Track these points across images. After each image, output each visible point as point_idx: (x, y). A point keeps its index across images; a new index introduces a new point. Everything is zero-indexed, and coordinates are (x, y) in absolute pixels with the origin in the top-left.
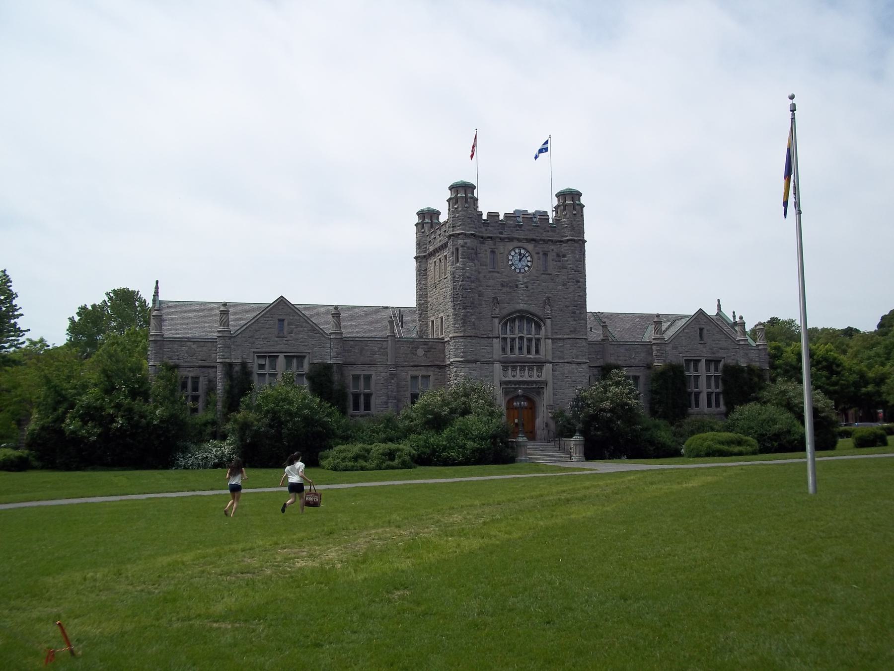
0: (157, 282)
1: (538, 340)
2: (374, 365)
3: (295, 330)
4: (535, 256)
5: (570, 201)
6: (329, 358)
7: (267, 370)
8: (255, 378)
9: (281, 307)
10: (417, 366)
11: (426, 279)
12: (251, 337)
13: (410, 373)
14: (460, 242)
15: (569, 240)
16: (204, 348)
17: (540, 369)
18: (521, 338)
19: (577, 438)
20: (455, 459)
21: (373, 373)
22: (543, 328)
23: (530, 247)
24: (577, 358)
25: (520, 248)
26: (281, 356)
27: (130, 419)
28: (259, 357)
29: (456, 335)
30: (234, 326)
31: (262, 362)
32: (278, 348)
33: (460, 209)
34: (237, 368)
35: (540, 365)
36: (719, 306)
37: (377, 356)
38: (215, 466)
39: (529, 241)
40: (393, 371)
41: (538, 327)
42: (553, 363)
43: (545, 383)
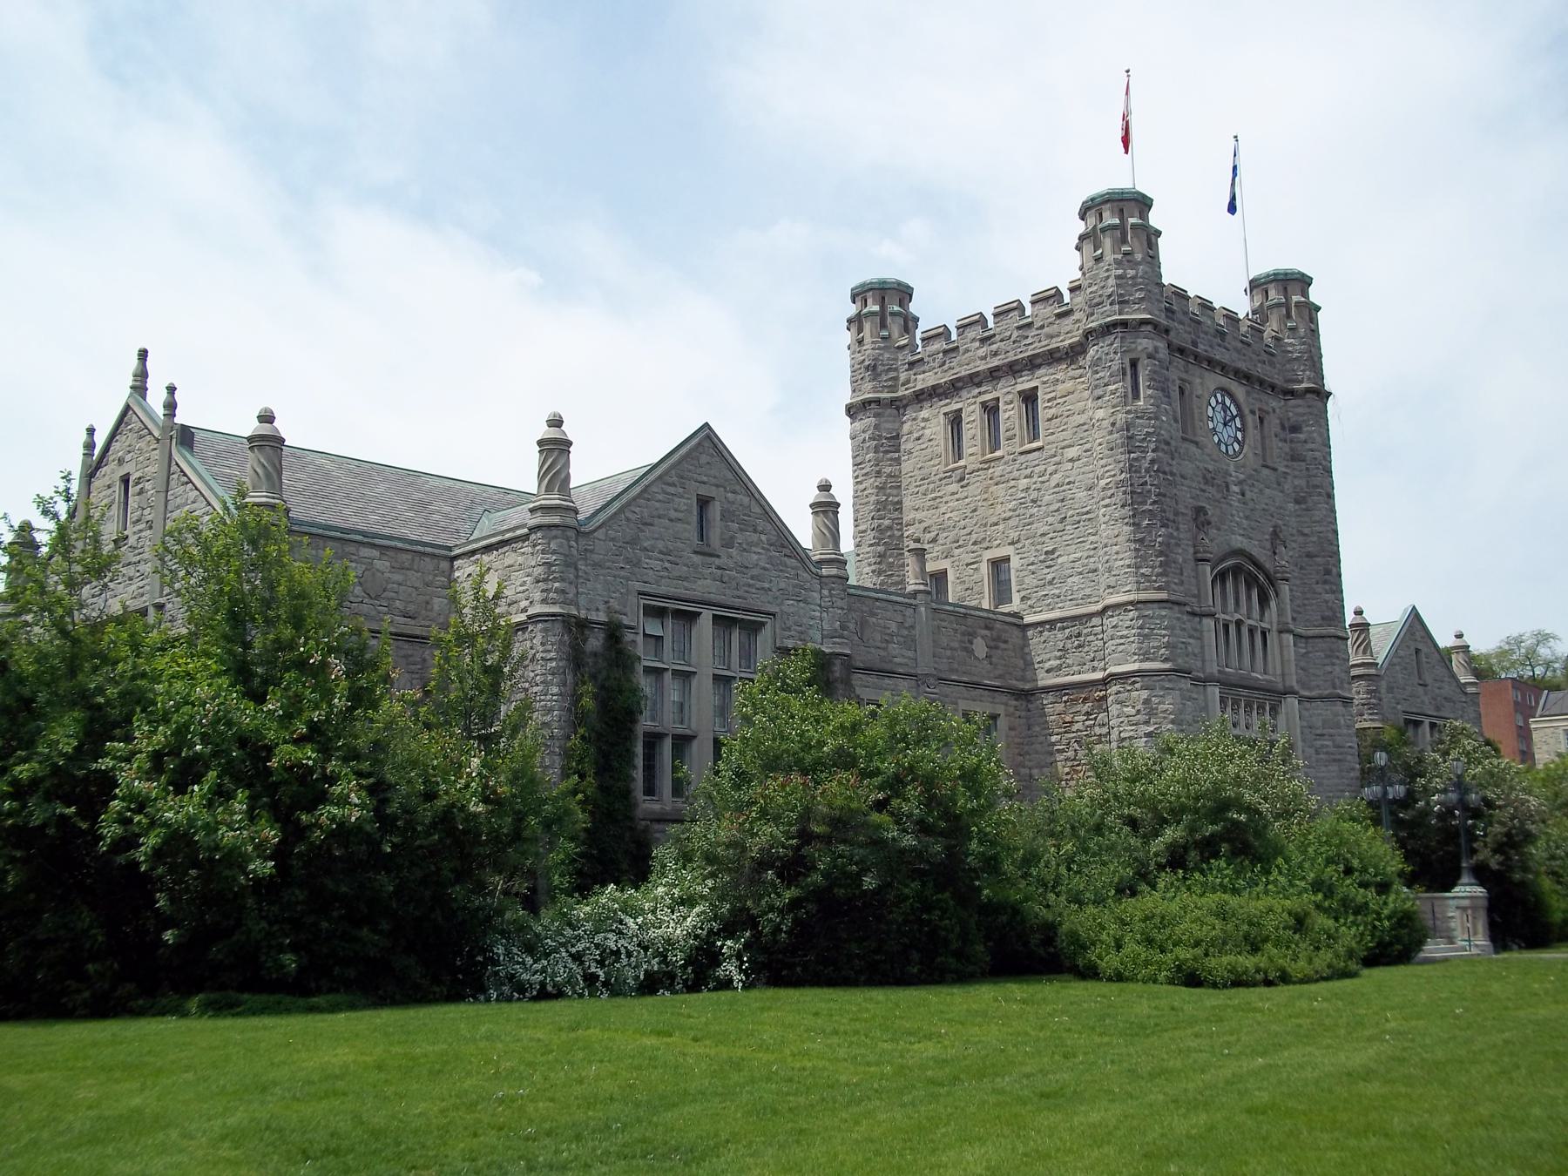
0: (143, 355)
2: (890, 673)
3: (740, 538)
4: (1249, 418)
5: (1287, 293)
6: (818, 637)
10: (975, 685)
11: (898, 461)
12: (633, 542)
13: (963, 705)
14: (1144, 343)
15: (1308, 390)
16: (413, 577)
18: (1239, 623)
19: (1468, 890)
22: (1273, 604)
23: (1239, 391)
25: (1226, 391)
27: (378, 790)
29: (1143, 596)
32: (705, 587)
33: (1138, 257)
34: (595, 642)
37: (894, 648)
38: (650, 985)
39: (1245, 377)
41: (1264, 601)
42: (1303, 700)
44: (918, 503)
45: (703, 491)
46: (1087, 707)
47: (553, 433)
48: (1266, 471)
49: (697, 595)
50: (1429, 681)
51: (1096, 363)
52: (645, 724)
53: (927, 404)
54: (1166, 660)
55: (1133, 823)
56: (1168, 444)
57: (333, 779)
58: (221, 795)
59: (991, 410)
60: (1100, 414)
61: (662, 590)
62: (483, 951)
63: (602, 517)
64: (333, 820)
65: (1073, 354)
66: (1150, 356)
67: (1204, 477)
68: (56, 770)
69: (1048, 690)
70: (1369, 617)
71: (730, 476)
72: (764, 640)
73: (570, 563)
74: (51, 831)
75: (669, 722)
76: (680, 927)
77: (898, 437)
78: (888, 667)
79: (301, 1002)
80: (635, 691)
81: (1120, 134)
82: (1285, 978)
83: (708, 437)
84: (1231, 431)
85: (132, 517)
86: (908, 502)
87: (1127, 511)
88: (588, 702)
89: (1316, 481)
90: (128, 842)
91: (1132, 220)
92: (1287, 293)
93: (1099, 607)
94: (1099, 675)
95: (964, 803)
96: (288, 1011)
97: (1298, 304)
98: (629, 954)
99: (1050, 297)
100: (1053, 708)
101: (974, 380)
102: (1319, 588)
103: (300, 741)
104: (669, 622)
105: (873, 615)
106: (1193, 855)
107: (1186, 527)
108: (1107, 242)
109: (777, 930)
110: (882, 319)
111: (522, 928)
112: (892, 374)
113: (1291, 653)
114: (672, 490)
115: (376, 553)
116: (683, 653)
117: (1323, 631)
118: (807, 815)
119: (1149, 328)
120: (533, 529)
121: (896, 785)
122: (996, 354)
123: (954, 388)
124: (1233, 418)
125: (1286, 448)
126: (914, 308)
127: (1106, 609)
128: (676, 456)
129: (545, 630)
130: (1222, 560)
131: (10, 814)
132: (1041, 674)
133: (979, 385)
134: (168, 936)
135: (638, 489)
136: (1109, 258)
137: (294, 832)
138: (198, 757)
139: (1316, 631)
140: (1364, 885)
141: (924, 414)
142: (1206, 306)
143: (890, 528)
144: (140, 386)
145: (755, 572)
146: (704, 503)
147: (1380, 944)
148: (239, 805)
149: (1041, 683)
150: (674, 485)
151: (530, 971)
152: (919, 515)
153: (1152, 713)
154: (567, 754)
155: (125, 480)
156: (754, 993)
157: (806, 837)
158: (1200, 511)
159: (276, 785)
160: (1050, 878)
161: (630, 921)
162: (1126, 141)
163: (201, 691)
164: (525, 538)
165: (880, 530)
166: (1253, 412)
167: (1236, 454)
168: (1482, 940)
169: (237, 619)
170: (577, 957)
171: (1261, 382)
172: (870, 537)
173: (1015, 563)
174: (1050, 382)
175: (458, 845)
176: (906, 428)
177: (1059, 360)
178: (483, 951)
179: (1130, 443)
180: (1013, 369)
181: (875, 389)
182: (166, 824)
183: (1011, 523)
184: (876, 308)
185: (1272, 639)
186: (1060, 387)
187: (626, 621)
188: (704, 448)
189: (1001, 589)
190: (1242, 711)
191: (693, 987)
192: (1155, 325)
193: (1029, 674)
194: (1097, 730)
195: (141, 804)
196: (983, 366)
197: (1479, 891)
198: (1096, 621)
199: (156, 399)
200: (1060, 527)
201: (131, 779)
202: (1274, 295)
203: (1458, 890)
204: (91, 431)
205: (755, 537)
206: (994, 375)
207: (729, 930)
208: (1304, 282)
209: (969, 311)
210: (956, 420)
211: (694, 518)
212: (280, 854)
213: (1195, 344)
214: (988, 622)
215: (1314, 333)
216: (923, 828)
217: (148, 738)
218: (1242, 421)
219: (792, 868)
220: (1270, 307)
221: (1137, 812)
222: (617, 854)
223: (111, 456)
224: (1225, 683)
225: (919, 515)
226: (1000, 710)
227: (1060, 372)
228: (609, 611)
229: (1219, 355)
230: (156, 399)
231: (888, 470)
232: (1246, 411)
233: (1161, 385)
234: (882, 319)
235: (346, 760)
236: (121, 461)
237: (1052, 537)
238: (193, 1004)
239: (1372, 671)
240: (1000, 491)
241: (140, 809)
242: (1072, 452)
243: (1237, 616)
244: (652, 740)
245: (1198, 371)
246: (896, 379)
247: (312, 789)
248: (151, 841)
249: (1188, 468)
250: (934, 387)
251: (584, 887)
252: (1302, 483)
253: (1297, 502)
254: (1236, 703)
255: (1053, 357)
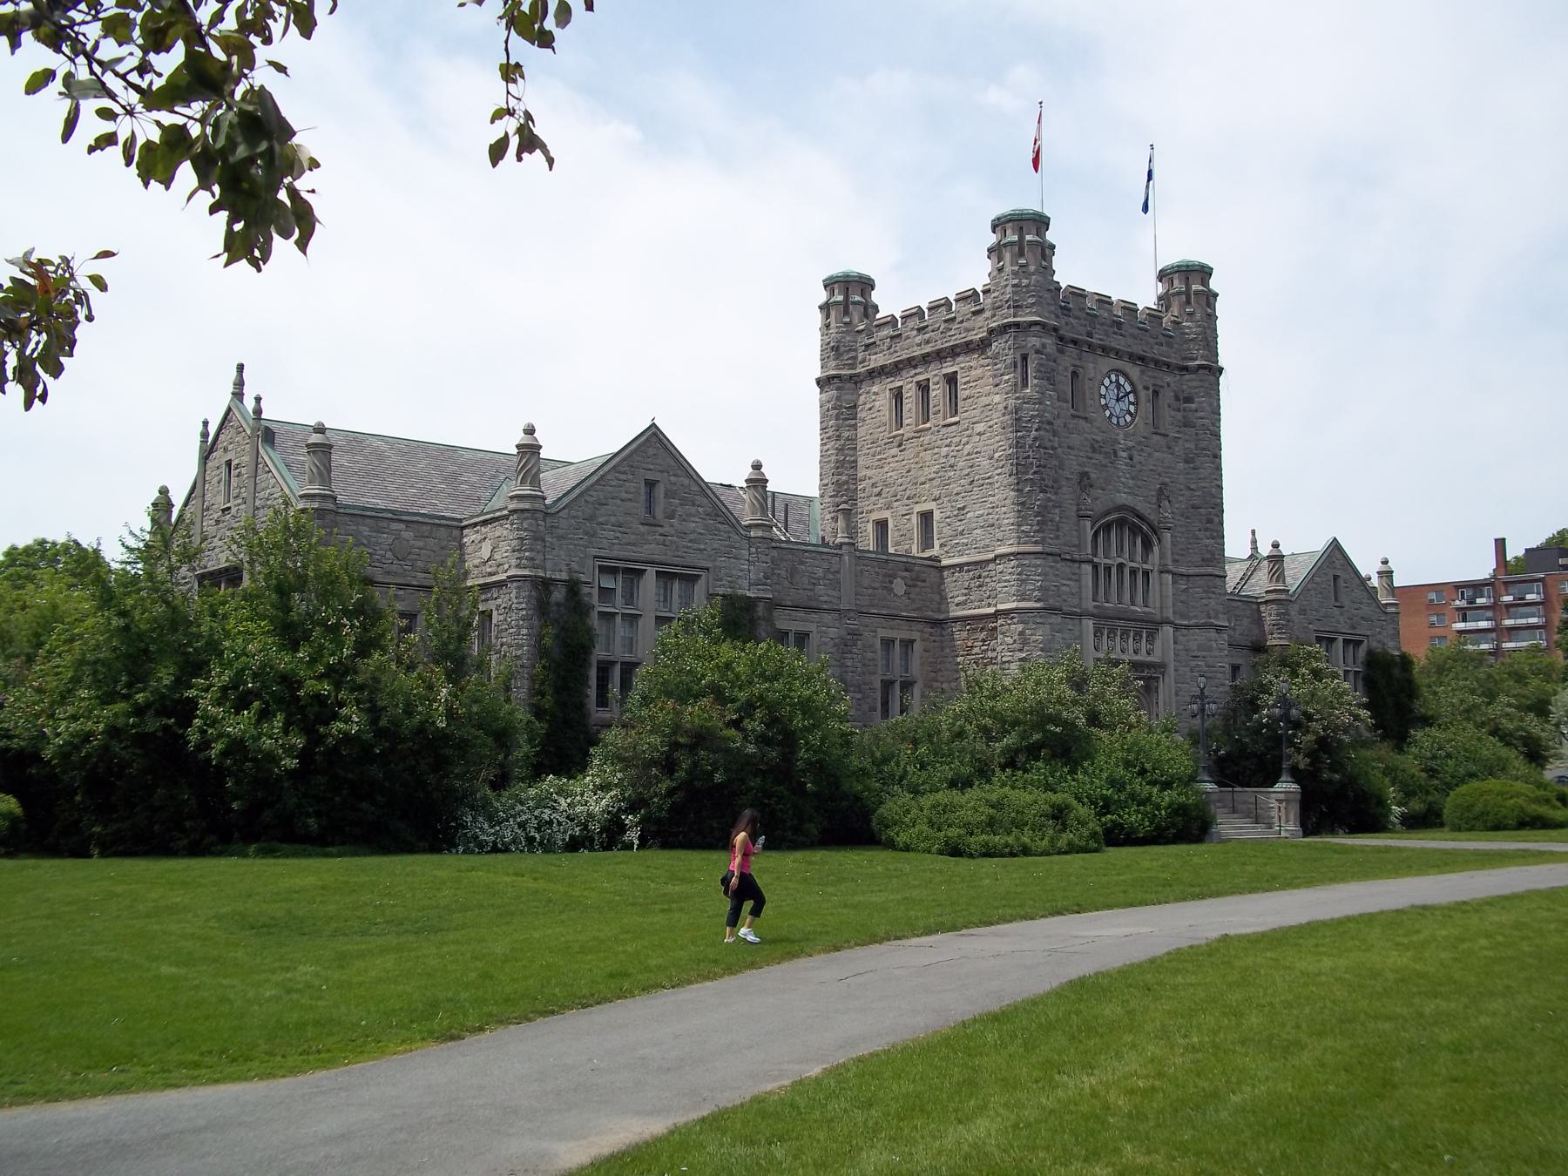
0: (241, 368)
1: (1146, 574)
3: (680, 511)
4: (1142, 394)
5: (1190, 285)
6: (745, 584)
7: (618, 606)
8: (594, 620)
9: (651, 451)
11: (855, 427)
12: (590, 518)
13: (882, 633)
14: (1034, 341)
15: (1201, 367)
16: (431, 541)
17: (1151, 638)
18: (1121, 566)
19: (1286, 786)
20: (1133, 830)
21: (812, 627)
22: (1156, 549)
23: (1134, 371)
24: (1216, 618)
25: (1119, 372)
26: (651, 572)
27: (374, 712)
28: (603, 569)
29: (1023, 548)
30: (553, 487)
31: (608, 582)
32: (650, 550)
33: (1032, 268)
34: (558, 595)
35: (1152, 626)
36: (1254, 542)
37: (820, 589)
38: (574, 845)
40: (854, 624)
41: (1147, 545)
42: (1177, 627)
43: (1161, 667)
44: (868, 463)
45: (650, 476)
46: (983, 635)
47: (528, 440)
48: (1156, 437)
49: (643, 556)
50: (1347, 603)
51: (996, 356)
52: (599, 653)
53: (877, 380)
54: (1038, 600)
55: (986, 731)
56: (1050, 423)
57: (341, 705)
58: (264, 715)
59: (924, 388)
60: (997, 398)
61: (614, 554)
62: (455, 819)
63: (566, 501)
64: (339, 732)
65: (982, 346)
66: (1037, 352)
67: (1092, 447)
68: (163, 696)
69: (956, 620)
70: (1285, 550)
71: (672, 463)
72: (700, 588)
73: (537, 538)
74: (160, 734)
75: (619, 653)
76: (599, 805)
77: (855, 406)
78: (814, 604)
79: (319, 850)
80: (589, 630)
81: (1031, 156)
82: (1026, 851)
83: (655, 434)
84: (1123, 405)
85: (234, 493)
86: (861, 462)
87: (1013, 479)
88: (548, 641)
89: (1203, 444)
90: (205, 744)
91: (1028, 237)
92: (1190, 285)
93: (991, 556)
94: (992, 610)
95: (798, 722)
96: (310, 855)
97: (1197, 293)
98: (559, 824)
99: (969, 297)
100: (960, 635)
101: (911, 363)
102: (1201, 535)
103: (320, 678)
104: (620, 578)
105: (802, 563)
106: (1022, 758)
107: (1067, 493)
108: (1007, 256)
109: (660, 809)
110: (846, 307)
111: (486, 803)
112: (852, 354)
113: (1170, 590)
114: (623, 477)
115: (402, 526)
116: (630, 598)
117: (1202, 570)
118: (677, 728)
119: (1038, 328)
120: (513, 512)
121: (749, 708)
122: (928, 342)
123: (896, 369)
124: (1127, 394)
125: (1179, 415)
126: (875, 297)
127: (996, 557)
128: (634, 446)
129: (518, 588)
130: (1107, 513)
131: (133, 726)
132: (952, 607)
133: (915, 367)
134: (234, 806)
135: (595, 478)
136: (1008, 269)
137: (314, 739)
138: (250, 692)
139: (1196, 571)
140: (1153, 783)
141: (875, 389)
142: (1104, 301)
143: (846, 482)
144: (238, 394)
145: (692, 537)
146: (651, 485)
147: (1158, 828)
148: (278, 722)
149: (952, 614)
150: (624, 473)
151: (487, 834)
152: (869, 473)
153: (1025, 642)
154: (532, 679)
155: (229, 463)
156: (648, 853)
157: (675, 746)
158: (1084, 475)
159: (304, 707)
160: (899, 772)
161: (562, 800)
162: (1036, 163)
163: (252, 645)
164: (506, 517)
165: (838, 484)
166: (1146, 388)
167: (1127, 425)
168: (1291, 827)
169: (283, 591)
170: (522, 825)
171: (1157, 362)
172: (830, 490)
173: (937, 516)
174: (971, 369)
175: (435, 748)
176: (862, 399)
177: (973, 351)
178: (455, 819)
179: (1018, 423)
180: (940, 356)
181: (837, 367)
182: (229, 735)
183: (935, 483)
184: (840, 298)
185: (1154, 577)
186: (974, 373)
187: (583, 578)
188: (653, 442)
189: (927, 542)
190: (1118, 639)
191: (607, 847)
192: (1043, 325)
193: (943, 607)
194: (990, 654)
195: (214, 722)
196: (918, 352)
197: (1294, 787)
198: (991, 566)
199: (249, 404)
200: (969, 488)
201: (206, 705)
202: (1178, 285)
203: (1279, 787)
204: (206, 423)
205: (693, 510)
206: (926, 359)
207: (632, 809)
208: (1204, 272)
209: (910, 304)
210: (898, 395)
211: (643, 498)
212: (305, 755)
213: (1090, 335)
214: (908, 565)
215: (1211, 318)
216: (763, 740)
217: (220, 677)
218: (1136, 397)
219: (669, 766)
220: (1174, 295)
221: (988, 721)
222: (565, 751)
223: (220, 445)
224: (1100, 617)
225: (869, 473)
226: (916, 635)
227: (974, 360)
228: (570, 571)
229: (1116, 342)
230: (249, 404)
231: (846, 434)
232: (1140, 387)
233: (1048, 376)
234: (846, 307)
235: (352, 690)
236: (226, 450)
237: (962, 495)
238: (253, 847)
239: (1283, 597)
240: (927, 456)
241: (212, 726)
242: (980, 428)
243: (1120, 560)
244: (605, 668)
245: (1091, 357)
246: (855, 358)
247: (326, 710)
248: (218, 747)
249: (1075, 439)
250: (883, 367)
251: (537, 772)
252: (1191, 445)
253: (1186, 462)
254: (1112, 631)
255: (968, 348)
